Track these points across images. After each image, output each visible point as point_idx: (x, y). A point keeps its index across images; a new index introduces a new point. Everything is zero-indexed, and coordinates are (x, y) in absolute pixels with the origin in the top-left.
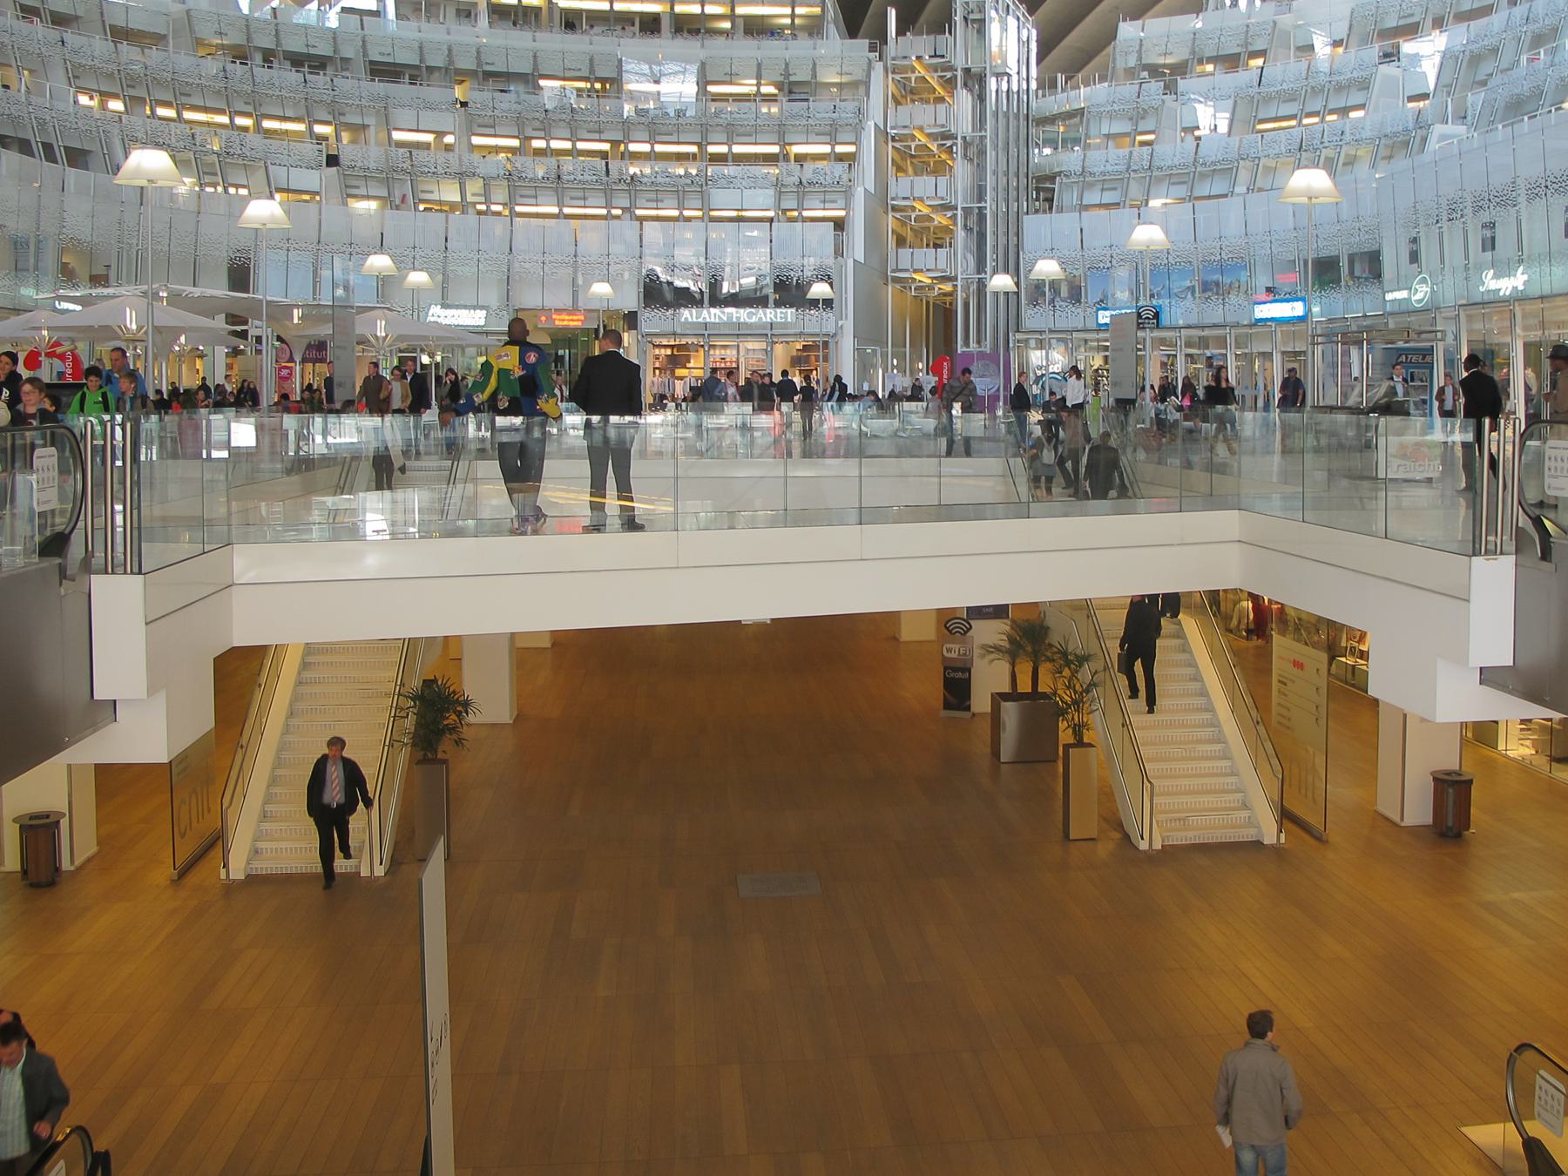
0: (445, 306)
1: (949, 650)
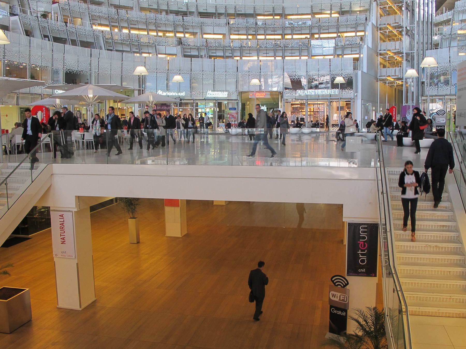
0: (214, 91)
1: (333, 296)
